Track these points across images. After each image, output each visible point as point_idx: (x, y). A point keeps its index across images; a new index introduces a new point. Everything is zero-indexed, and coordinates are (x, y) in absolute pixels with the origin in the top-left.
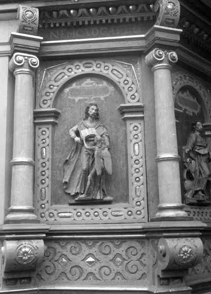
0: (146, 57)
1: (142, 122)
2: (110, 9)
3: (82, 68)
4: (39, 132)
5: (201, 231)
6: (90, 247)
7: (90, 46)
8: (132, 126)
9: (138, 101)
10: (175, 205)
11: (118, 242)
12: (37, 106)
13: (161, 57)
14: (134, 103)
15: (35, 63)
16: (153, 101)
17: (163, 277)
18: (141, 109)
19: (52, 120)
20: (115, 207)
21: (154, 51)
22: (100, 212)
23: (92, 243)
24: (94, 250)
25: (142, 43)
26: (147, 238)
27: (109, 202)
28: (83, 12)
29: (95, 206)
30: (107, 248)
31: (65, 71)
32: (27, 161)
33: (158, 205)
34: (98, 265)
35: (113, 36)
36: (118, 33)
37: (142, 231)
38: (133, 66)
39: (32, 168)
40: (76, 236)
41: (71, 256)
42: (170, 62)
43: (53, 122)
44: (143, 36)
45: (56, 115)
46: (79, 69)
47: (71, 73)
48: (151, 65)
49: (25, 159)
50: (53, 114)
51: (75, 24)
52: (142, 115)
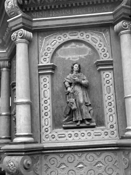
1: (112, 72)
4: (42, 79)
5: (25, 152)
7: (67, 21)
9: (109, 58)
12: (40, 63)
13: (126, 27)
14: (106, 59)
16: (120, 58)
19: (51, 71)
21: (122, 22)
22: (86, 133)
23: (100, 153)
25: (111, 18)
27: (93, 127)
29: (68, 130)
31: (56, 39)
32: (26, 101)
33: (127, 127)
35: (40, 18)
36: (78, 13)
39: (29, 106)
44: (111, 13)
45: (53, 68)
46: (69, 37)
47: (61, 40)
48: (118, 35)
50: (51, 67)
51: (95, 3)
52: (112, 67)
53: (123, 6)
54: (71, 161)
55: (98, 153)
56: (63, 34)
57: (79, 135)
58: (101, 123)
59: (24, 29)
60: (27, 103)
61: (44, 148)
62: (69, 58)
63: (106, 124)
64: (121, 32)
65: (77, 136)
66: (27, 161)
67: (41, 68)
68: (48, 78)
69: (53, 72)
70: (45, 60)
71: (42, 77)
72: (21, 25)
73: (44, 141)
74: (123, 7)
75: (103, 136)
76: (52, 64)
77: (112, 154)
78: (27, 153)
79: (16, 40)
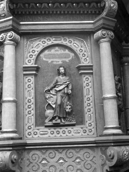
0: (95, 34)
1: (91, 76)
2: (50, 5)
3: (63, 40)
5: (113, 143)
6: (77, 152)
8: (27, 79)
10: (11, 130)
11: (61, 150)
12: (25, 63)
14: (86, 63)
15: (10, 35)
17: (110, 170)
18: (90, 68)
19: (35, 73)
20: (76, 128)
23: (45, 150)
24: (63, 155)
25: (91, 26)
26: (96, 147)
27: (73, 125)
28: (33, 6)
30: (71, 154)
33: (105, 126)
34: (66, 164)
37: (94, 142)
38: (84, 41)
40: (86, 145)
41: (49, 159)
42: (110, 38)
43: (35, 74)
44: (92, 22)
45: (37, 69)
46: (53, 41)
48: (97, 42)
49: (11, 99)
52: (92, 72)
53: (102, 17)
54: (53, 157)
55: (77, 150)
56: (47, 38)
57: (61, 132)
58: (81, 122)
59: (14, 32)
60: (14, 101)
61: (26, 143)
62: (52, 62)
63: (37, 128)
64: (101, 40)
65: (64, 133)
66: (14, 156)
67: (26, 69)
68: (32, 79)
69: (37, 73)
70: (29, 61)
71: (26, 78)
72: (11, 27)
73: (26, 138)
74: (103, 18)
75: (82, 133)
76: (37, 65)
77: (89, 151)
78: (15, 148)
79: (4, 41)
